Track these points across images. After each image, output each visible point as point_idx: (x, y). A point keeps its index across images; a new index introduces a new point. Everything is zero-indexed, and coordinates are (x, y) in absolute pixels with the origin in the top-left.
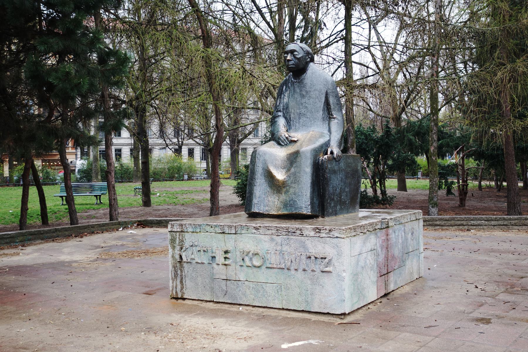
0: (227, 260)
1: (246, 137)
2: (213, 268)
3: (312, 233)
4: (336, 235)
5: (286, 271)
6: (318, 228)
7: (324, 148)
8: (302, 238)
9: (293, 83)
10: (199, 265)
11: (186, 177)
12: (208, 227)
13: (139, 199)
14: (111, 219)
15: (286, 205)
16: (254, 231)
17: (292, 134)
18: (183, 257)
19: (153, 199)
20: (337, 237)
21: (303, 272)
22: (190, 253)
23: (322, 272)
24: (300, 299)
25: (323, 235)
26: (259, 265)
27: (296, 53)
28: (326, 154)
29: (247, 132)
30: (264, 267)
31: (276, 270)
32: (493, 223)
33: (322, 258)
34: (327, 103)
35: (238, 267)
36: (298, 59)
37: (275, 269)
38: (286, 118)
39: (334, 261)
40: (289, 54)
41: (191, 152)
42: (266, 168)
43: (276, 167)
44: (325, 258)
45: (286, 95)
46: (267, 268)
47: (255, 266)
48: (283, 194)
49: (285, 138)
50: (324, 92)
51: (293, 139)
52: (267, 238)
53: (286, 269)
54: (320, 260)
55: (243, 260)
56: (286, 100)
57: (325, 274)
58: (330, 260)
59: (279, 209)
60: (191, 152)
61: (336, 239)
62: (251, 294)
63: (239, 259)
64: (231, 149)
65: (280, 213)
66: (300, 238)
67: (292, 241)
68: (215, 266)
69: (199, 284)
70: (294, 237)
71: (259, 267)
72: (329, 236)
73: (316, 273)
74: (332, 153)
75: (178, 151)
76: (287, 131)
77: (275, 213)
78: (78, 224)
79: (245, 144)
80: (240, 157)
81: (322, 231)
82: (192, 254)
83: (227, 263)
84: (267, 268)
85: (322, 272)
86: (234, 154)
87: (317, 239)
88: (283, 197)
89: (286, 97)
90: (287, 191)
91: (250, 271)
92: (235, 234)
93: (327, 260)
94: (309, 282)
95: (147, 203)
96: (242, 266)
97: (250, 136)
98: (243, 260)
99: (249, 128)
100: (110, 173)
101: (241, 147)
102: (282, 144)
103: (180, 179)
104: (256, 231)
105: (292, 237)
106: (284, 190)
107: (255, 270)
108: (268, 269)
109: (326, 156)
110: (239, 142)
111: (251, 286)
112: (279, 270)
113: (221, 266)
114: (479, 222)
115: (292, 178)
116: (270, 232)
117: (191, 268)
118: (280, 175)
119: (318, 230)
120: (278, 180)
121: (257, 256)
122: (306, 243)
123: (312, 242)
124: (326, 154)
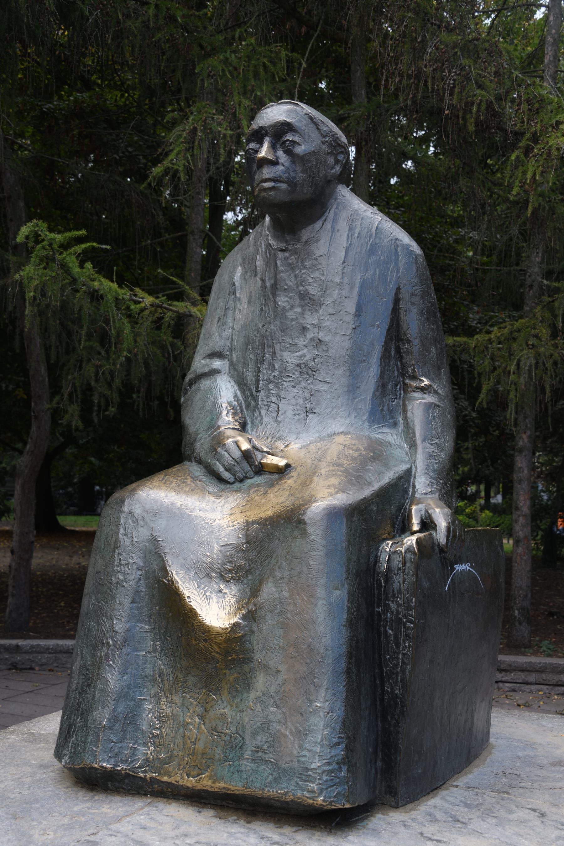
7: (382, 512)
27: (289, 137)
28: (405, 528)
74: (427, 524)
102: (226, 475)
109: (411, 541)
118: (216, 610)
124: (405, 528)
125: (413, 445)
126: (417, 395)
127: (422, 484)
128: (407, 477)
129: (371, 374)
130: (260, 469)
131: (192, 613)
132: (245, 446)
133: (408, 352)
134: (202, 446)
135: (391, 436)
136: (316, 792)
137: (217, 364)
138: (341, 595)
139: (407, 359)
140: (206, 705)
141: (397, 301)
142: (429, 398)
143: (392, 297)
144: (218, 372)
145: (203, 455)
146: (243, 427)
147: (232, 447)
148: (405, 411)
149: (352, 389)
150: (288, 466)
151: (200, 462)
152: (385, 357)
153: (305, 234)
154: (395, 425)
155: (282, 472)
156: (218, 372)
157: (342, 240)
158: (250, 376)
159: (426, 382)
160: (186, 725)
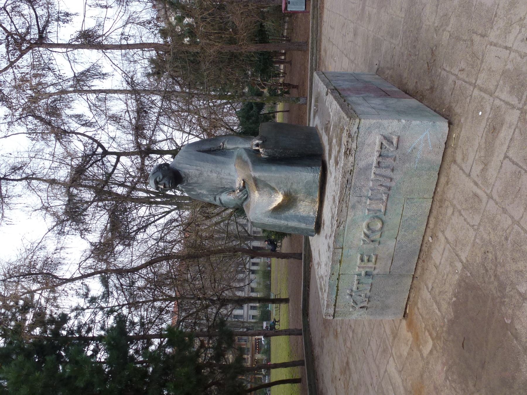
0: (370, 259)
1: (246, 231)
2: (377, 274)
3: (351, 159)
4: (355, 129)
5: (391, 192)
6: (345, 153)
7: (254, 155)
8: (355, 171)
9: (189, 184)
10: (373, 289)
11: (269, 269)
12: (333, 277)
13: (283, 306)
14: (301, 334)
15: (309, 194)
16: (341, 228)
17: (237, 186)
18: (362, 305)
19: (283, 296)
20: (358, 128)
21: (395, 172)
22: (358, 298)
23: (397, 148)
24: (425, 177)
25: (354, 146)
26: (381, 223)
27: (158, 180)
28: (258, 151)
29: (243, 230)
30: (384, 218)
31: (388, 203)
32: (315, 51)
33: (381, 148)
34: (209, 151)
35: (380, 247)
36: (163, 177)
37: (388, 205)
38: (222, 192)
39: (386, 133)
40: (159, 186)
41: (254, 264)
42: (270, 212)
43: (270, 204)
44: (382, 144)
45: (200, 191)
46: (385, 215)
47: (382, 228)
48: (298, 195)
49: (240, 193)
50: (197, 152)
51: (242, 185)
52: (351, 213)
53: (389, 192)
54: (383, 150)
55: (373, 241)
56: (204, 192)
57: (400, 144)
58: (385, 138)
59: (313, 201)
60: (254, 264)
61: (360, 130)
62: (412, 233)
63: (372, 246)
64: (253, 240)
65: (317, 200)
66: (354, 174)
67: (358, 184)
68: (375, 272)
69: (393, 289)
70: (353, 181)
71: (383, 224)
72: (355, 138)
73: (397, 156)
74: (257, 145)
75: (253, 272)
76: (234, 191)
77: (318, 205)
78: (303, 361)
79: (251, 232)
80: (258, 235)
81: (349, 147)
82: (360, 296)
83: (373, 260)
84: (385, 215)
85: (397, 148)
86: (256, 238)
87: (358, 153)
88: (301, 196)
89: (202, 191)
90: (296, 192)
91: (386, 233)
92: (342, 248)
93: (384, 142)
94: (407, 165)
95: (286, 301)
96: (379, 242)
97: (246, 228)
98: (373, 241)
99: (240, 229)
100: (266, 334)
101: (252, 235)
102: (246, 196)
103: (269, 272)
104: (342, 226)
105: (353, 184)
106: (293, 194)
107: (385, 228)
108: (386, 214)
109: (261, 150)
110: (249, 235)
111: (403, 233)
112: (389, 201)
113: (377, 266)
114: (314, 61)
115: (282, 186)
116: (344, 209)
117: (375, 298)
118: (279, 199)
119: (348, 153)
120: (283, 200)
121: (370, 225)
122: (361, 167)
123: (361, 160)
124: (258, 151)
125: (238, 148)
126: (225, 146)
127: (247, 146)
128: (245, 149)
129: (219, 158)
130: (244, 187)
131: (279, 204)
132: (238, 191)
133: (214, 148)
134: (239, 202)
135: (236, 153)
136: (317, 176)
137: (217, 198)
138: (274, 168)
139: (215, 149)
140: (301, 200)
141: (200, 151)
142: (226, 143)
143: (199, 153)
144: (219, 199)
145: (241, 202)
146: (234, 191)
147: (239, 194)
148: (229, 149)
149: (223, 163)
150: (243, 180)
151: (243, 203)
152: (216, 154)
153: (183, 176)
154: (233, 152)
155: (244, 182)
156: (219, 199)
157: (185, 166)
158: (221, 190)
159: (221, 144)
160: (305, 205)
